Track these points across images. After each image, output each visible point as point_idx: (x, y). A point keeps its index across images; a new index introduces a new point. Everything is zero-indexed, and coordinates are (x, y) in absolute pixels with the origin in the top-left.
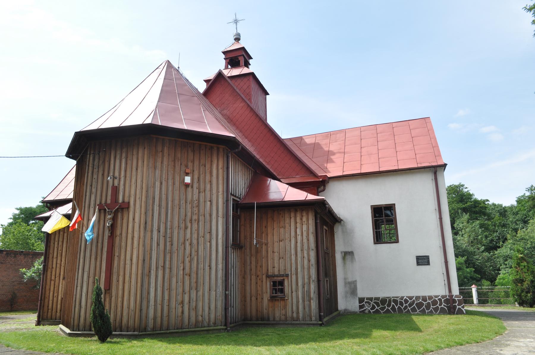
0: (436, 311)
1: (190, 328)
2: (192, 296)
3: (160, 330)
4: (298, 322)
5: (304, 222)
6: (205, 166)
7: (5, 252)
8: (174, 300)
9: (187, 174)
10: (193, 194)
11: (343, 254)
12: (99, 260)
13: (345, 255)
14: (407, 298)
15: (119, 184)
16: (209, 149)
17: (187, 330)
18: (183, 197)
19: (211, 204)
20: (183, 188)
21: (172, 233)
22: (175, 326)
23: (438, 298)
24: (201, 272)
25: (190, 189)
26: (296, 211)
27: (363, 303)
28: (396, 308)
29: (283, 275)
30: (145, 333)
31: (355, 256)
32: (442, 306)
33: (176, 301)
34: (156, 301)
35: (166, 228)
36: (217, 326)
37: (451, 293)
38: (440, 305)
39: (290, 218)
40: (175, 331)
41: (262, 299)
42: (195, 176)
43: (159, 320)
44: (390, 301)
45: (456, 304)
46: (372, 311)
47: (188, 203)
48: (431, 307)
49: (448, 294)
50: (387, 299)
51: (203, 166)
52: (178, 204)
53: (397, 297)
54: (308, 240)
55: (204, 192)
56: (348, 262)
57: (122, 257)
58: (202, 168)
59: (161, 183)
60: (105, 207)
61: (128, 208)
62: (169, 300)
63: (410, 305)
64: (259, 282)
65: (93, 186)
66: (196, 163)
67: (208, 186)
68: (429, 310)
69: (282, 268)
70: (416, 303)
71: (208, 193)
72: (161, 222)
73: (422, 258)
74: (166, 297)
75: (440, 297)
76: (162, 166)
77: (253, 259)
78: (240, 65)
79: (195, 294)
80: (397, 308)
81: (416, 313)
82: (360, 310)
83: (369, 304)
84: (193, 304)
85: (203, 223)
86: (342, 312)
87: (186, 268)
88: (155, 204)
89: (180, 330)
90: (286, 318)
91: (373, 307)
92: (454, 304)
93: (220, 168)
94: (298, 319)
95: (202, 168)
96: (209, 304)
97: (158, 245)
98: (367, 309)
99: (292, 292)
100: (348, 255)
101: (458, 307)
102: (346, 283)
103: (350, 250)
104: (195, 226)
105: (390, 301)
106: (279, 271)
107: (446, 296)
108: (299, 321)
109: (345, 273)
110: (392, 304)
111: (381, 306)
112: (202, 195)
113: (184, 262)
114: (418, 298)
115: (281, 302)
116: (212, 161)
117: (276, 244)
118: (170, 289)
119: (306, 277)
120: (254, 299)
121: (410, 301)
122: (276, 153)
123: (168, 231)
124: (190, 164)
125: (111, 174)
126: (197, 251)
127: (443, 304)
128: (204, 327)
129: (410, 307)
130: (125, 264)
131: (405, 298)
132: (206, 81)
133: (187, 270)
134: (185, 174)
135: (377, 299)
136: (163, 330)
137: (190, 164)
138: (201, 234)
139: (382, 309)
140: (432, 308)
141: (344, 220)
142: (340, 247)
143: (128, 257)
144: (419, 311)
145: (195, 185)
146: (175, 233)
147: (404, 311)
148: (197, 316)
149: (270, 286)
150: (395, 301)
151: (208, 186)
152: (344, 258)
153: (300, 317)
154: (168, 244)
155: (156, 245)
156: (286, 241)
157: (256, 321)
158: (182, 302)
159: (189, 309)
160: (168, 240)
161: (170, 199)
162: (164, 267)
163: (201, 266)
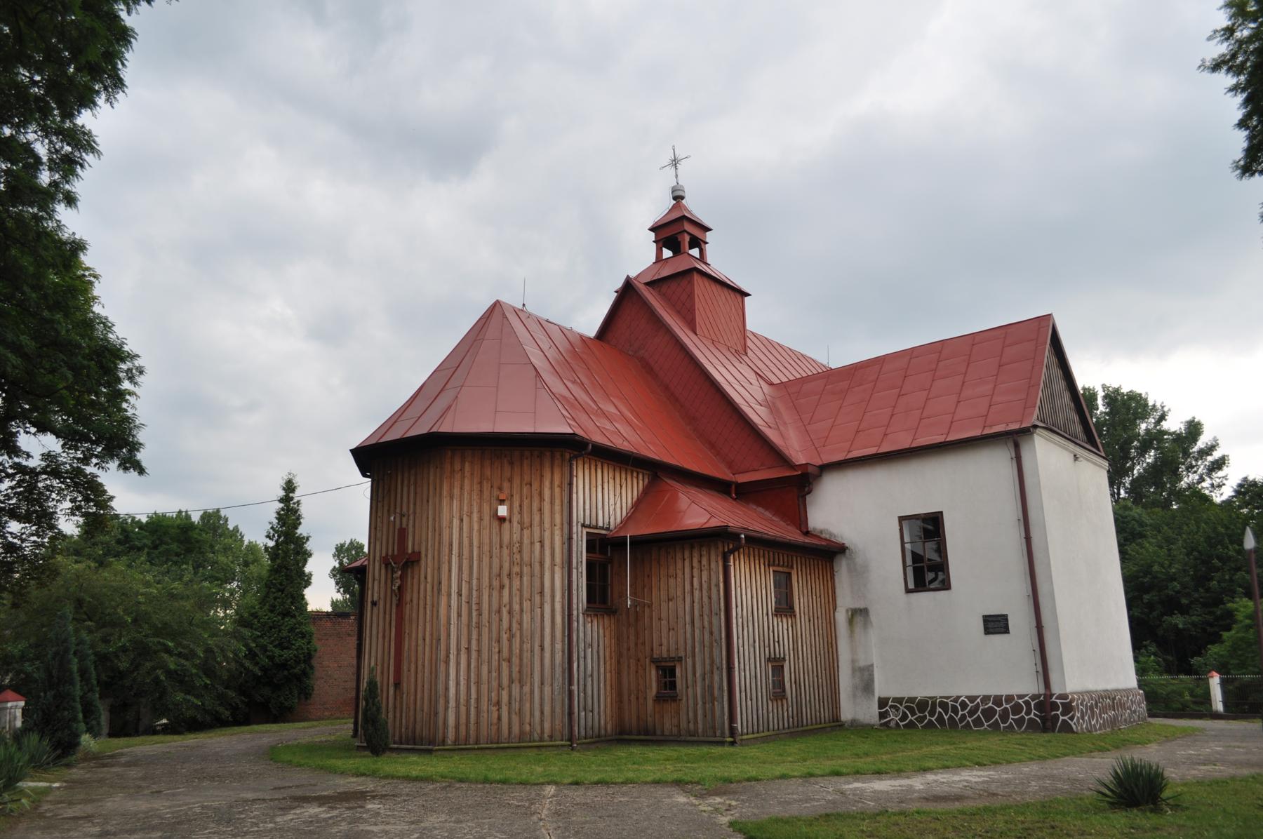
0: (1020, 727)
1: (512, 743)
2: (513, 693)
3: (466, 744)
4: (695, 738)
5: (704, 566)
6: (531, 485)
7: (353, 615)
8: (486, 699)
9: (502, 502)
10: (511, 533)
11: (850, 613)
12: (387, 640)
13: (852, 615)
14: (966, 700)
15: (408, 525)
16: (538, 457)
17: (506, 745)
18: (496, 539)
19: (542, 546)
20: (496, 524)
21: (480, 597)
22: (488, 739)
23: (1023, 700)
24: (526, 655)
25: (506, 525)
26: (692, 547)
27: (885, 709)
28: (946, 718)
29: (674, 658)
30: (443, 747)
31: (871, 617)
32: (1032, 716)
33: (488, 701)
34: (458, 700)
35: (470, 590)
36: (555, 741)
37: (1050, 690)
38: (1028, 713)
39: (684, 560)
40: (487, 746)
41: (646, 698)
42: (515, 503)
43: (463, 729)
44: (934, 704)
45: (1059, 713)
46: (901, 724)
47: (505, 548)
48: (1011, 716)
49: (1042, 691)
50: (928, 701)
51: (528, 486)
52: (488, 549)
53: (947, 698)
54: (710, 598)
55: (530, 529)
56: (858, 629)
57: (414, 636)
58: (525, 490)
59: (461, 520)
60: (391, 561)
61: (418, 561)
62: (478, 700)
63: (972, 713)
64: (641, 671)
65: (378, 528)
66: (517, 481)
67: (536, 518)
68: (1006, 723)
69: (673, 647)
70: (982, 709)
71: (536, 529)
72: (464, 581)
73: (994, 619)
74: (474, 696)
75: (1027, 698)
76: (461, 495)
77: (632, 631)
78: (680, 251)
79: (518, 690)
80: (948, 719)
81: (982, 728)
82: (880, 721)
83: (897, 711)
84: (516, 706)
85: (529, 578)
86: (848, 725)
87: (504, 650)
88: (454, 553)
89: (495, 746)
90: (679, 731)
91: (904, 717)
92: (1053, 713)
93: (556, 486)
94: (695, 733)
95: (525, 490)
96: (542, 705)
97: (459, 615)
98: (893, 719)
99: (687, 687)
100: (859, 615)
101: (1061, 718)
102: (854, 670)
103: (862, 607)
104: (516, 583)
105: (934, 704)
106: (668, 651)
107: (1039, 696)
108: (698, 736)
109: (853, 650)
110: (937, 711)
111: (919, 714)
112: (526, 532)
113: (499, 642)
114: (986, 699)
115: (672, 704)
116: (542, 476)
117: (664, 605)
118: (478, 683)
119: (707, 661)
120: (633, 697)
121: (971, 705)
122: (725, 426)
123: (475, 593)
124: (506, 485)
125: (398, 510)
126: (520, 623)
127: (1033, 711)
128: (534, 741)
129: (970, 717)
130: (417, 645)
131: (962, 698)
132: (616, 292)
133: (505, 653)
134: (498, 502)
135: (911, 700)
136: (469, 744)
137: (506, 485)
138: (526, 594)
139: (921, 719)
140: (1012, 719)
141: (852, 547)
142: (845, 600)
143: (420, 635)
144: (987, 726)
145: (516, 519)
146: (484, 597)
147: (960, 725)
148: (521, 724)
149: (658, 677)
150: (944, 705)
151: (536, 518)
152: (851, 621)
153: (700, 731)
154: (474, 614)
155: (456, 615)
156: (678, 599)
157: (637, 735)
158: (498, 703)
159: (509, 713)
160: (474, 607)
161: (475, 543)
162: (468, 649)
163: (527, 646)
